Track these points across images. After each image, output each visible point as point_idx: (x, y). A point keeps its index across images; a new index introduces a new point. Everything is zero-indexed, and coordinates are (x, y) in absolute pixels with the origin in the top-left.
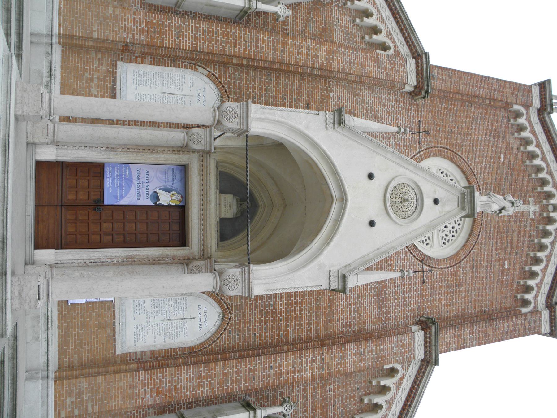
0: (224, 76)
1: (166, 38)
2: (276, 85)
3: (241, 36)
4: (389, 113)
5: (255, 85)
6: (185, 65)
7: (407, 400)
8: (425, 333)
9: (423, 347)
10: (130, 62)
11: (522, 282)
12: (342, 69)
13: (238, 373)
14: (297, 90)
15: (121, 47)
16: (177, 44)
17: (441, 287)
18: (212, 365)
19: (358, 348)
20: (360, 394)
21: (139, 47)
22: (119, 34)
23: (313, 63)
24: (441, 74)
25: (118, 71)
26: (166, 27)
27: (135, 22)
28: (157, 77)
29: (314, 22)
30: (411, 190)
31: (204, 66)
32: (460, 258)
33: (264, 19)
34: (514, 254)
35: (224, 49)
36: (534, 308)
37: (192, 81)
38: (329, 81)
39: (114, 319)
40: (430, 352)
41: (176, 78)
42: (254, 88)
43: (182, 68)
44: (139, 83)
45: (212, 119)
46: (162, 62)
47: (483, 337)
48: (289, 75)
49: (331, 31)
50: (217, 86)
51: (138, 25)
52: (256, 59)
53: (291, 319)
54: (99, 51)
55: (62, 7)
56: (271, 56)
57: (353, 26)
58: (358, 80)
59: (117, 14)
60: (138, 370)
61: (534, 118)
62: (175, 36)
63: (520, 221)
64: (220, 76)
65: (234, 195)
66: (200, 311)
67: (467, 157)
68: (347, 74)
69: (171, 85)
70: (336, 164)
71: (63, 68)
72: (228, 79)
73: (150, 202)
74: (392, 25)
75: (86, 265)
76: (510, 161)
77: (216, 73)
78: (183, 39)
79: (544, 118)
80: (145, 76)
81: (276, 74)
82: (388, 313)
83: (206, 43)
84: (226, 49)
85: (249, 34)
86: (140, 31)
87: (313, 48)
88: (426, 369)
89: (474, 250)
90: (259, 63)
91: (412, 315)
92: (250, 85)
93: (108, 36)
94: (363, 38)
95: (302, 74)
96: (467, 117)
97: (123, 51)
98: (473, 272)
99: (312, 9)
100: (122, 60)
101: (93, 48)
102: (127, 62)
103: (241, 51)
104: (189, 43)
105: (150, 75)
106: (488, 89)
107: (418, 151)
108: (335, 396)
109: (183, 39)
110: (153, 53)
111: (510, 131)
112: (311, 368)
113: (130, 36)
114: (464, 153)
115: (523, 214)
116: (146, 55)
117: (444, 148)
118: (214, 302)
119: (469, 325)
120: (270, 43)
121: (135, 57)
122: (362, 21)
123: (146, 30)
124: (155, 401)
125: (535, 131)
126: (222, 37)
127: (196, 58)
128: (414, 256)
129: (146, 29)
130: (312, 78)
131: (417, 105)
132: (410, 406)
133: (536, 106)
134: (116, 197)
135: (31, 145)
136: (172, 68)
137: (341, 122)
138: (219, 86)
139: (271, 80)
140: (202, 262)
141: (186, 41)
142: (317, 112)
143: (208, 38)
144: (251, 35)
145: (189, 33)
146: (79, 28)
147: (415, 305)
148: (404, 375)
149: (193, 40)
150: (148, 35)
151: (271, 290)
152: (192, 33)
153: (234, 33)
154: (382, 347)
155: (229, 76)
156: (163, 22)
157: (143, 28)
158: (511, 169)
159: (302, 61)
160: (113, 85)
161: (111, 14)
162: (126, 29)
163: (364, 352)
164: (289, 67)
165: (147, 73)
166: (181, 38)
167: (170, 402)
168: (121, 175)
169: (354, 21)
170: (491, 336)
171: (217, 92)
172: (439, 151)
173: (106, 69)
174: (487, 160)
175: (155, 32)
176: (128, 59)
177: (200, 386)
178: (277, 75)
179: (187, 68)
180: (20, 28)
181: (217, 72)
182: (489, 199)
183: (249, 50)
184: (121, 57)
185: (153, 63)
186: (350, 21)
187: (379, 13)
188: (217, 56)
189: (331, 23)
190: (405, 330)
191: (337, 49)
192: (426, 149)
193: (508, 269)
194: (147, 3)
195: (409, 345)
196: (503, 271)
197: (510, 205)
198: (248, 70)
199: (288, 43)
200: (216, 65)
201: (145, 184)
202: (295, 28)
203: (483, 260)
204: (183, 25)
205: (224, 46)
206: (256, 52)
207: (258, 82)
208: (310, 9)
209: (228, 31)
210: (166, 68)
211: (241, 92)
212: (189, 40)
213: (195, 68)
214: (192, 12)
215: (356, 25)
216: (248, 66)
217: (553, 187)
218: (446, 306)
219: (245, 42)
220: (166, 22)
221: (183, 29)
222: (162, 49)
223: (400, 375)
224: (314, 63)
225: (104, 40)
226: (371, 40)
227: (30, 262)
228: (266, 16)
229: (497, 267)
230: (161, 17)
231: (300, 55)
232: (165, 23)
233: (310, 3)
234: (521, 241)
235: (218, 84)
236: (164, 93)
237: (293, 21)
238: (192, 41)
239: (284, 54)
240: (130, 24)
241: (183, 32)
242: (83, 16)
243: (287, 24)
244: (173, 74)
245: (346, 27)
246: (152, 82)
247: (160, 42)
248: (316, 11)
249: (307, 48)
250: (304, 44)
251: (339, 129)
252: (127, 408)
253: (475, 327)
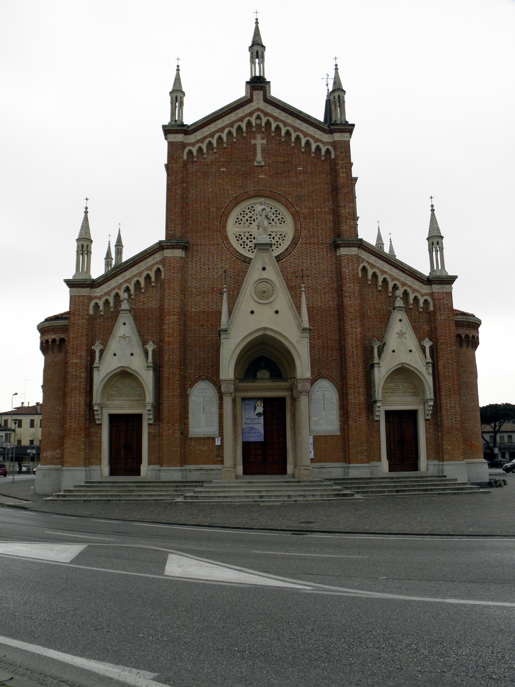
4: (201, 268)
7: (382, 260)
8: (342, 247)
9: (351, 248)
11: (313, 155)
13: (354, 372)
17: (313, 229)
18: (348, 386)
19: (347, 297)
20: (376, 292)
24: (171, 228)
25: (194, 436)
27: (169, 430)
30: (259, 286)
32: (294, 212)
34: (293, 160)
36: (331, 146)
39: (322, 436)
40: (353, 244)
45: (230, 397)
47: (348, 197)
50: (196, 382)
53: (327, 337)
57: (146, 293)
60: (348, 424)
61: (192, 138)
63: (269, 154)
65: (257, 371)
66: (320, 391)
67: (225, 203)
70: (247, 333)
71: (196, 464)
73: (262, 418)
74: (143, 266)
75: (295, 450)
76: (225, 161)
79: (191, 130)
82: (327, 272)
88: (365, 246)
89: (289, 199)
91: (330, 252)
94: (153, 286)
96: (196, 201)
98: (304, 200)
106: (176, 185)
107: (223, 245)
108: (375, 309)
111: (203, 160)
112: (356, 328)
113: (177, 431)
114: (223, 206)
115: (263, 150)
117: (220, 223)
118: (315, 383)
119: (339, 209)
124: (364, 416)
125: (202, 138)
128: (293, 250)
131: (193, 245)
132: (386, 258)
133: (182, 138)
134: (260, 435)
135: (237, 477)
137: (226, 331)
140: (294, 391)
142: (221, 343)
147: (324, 250)
148: (367, 262)
151: (308, 368)
154: (348, 279)
158: (230, 162)
162: (173, 434)
163: (349, 292)
167: (366, 408)
168: (248, 433)
169: (143, 293)
170: (348, 189)
171: (200, 382)
172: (222, 228)
174: (226, 184)
177: (359, 393)
182: (261, 227)
185: (187, 418)
190: (339, 259)
192: (222, 239)
193: (303, 167)
195: (348, 258)
196: (304, 172)
197: (264, 211)
201: (252, 420)
203: (296, 191)
210: (189, 411)
217: (243, 122)
218: (326, 225)
223: (366, 265)
227: (293, 476)
229: (301, 177)
234: (283, 154)
236: (204, 412)
245: (148, 299)
251: (229, 331)
252: (367, 430)
253: (341, 204)
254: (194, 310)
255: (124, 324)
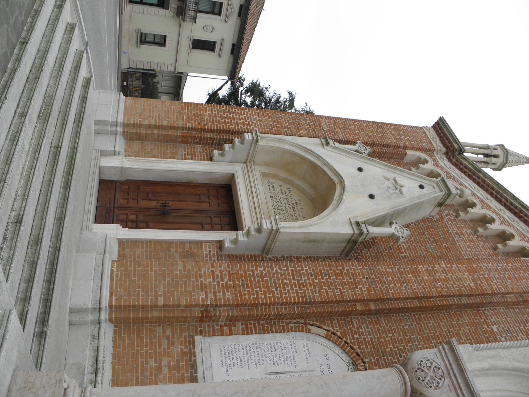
0: (348, 332)
1: (261, 290)
2: (420, 331)
3: (359, 273)
5: (394, 336)
6: (291, 327)
10: (214, 335)
12: (496, 288)
14: (449, 332)
15: (198, 314)
16: (278, 297)
21: (223, 310)
22: (194, 295)
23: (458, 288)
25: (198, 350)
26: (258, 277)
28: (255, 351)
29: (433, 243)
31: (318, 324)
33: (374, 250)
35: (341, 293)
37: (306, 348)
38: (483, 311)
41: (283, 348)
42: (393, 341)
43: (288, 332)
44: (230, 364)
46: (260, 329)
48: (432, 314)
49: (456, 248)
50: (343, 348)
51: (220, 280)
52: (387, 299)
54: (167, 325)
55: (115, 270)
56: (405, 291)
58: (520, 299)
59: (189, 270)
62: (272, 288)
64: (344, 334)
68: (504, 294)
69: (278, 360)
72: (355, 336)
77: (337, 331)
78: (284, 289)
80: (238, 353)
81: (414, 316)
83: (315, 289)
84: (344, 292)
85: (368, 268)
86: (223, 288)
87: (450, 271)
90: (391, 303)
92: (387, 339)
93: (179, 299)
94: (495, 249)
95: (448, 308)
97: (201, 320)
99: (424, 229)
100: (201, 334)
101: (159, 321)
102: (209, 336)
103: (365, 291)
104: (293, 293)
105: (244, 350)
109: (284, 289)
110: (245, 316)
113: (211, 295)
116: (235, 321)
120: (397, 275)
121: (219, 327)
122: (486, 228)
123: (231, 285)
126: (334, 278)
127: (306, 313)
129: (231, 283)
130: (460, 311)
136: (274, 334)
138: (346, 349)
139: (412, 326)
141: (288, 290)
143: (316, 282)
144: (370, 269)
145: (290, 280)
146: (138, 294)
149: (298, 288)
150: (235, 290)
152: (294, 279)
153: (348, 270)
155: (355, 331)
156: (253, 271)
157: (226, 283)
159: (444, 290)
160: (191, 373)
161: (180, 271)
162: (203, 287)
164: (430, 301)
165: (241, 347)
166: (280, 288)
169: (476, 232)
171: (346, 358)
173: (179, 350)
175: (243, 285)
176: (209, 331)
178: (417, 317)
179: (296, 331)
180: (49, 292)
181: (338, 328)
183: (374, 288)
184: (199, 329)
185: (246, 332)
186: (472, 233)
187: (500, 216)
188: (334, 306)
189: (452, 240)
191: (478, 266)
194: (225, 255)
198: (378, 318)
199: (419, 271)
200: (334, 320)
202: (415, 253)
204: (279, 271)
205: (340, 289)
206: (384, 289)
207: (396, 332)
208: (422, 229)
209: (341, 270)
210: (266, 336)
211: (379, 352)
212: (292, 289)
213: (306, 330)
214: (285, 256)
215: (480, 236)
216: (378, 312)
219: (365, 280)
220: (257, 270)
221: (281, 275)
222: (257, 309)
224: (460, 290)
225: (173, 306)
226: (506, 249)
228: (376, 246)
230: (248, 265)
231: (439, 282)
232: (256, 272)
233: (419, 223)
235: (343, 346)
236: (270, 374)
237: (409, 246)
238: (296, 290)
239: (420, 285)
240: (208, 280)
241: (282, 280)
242: (144, 278)
243: (403, 251)
244: (277, 343)
246: (250, 361)
247: (254, 298)
248: (430, 230)
249: (443, 272)
250: (438, 268)
254: (495, 328)
255: (421, 187)
